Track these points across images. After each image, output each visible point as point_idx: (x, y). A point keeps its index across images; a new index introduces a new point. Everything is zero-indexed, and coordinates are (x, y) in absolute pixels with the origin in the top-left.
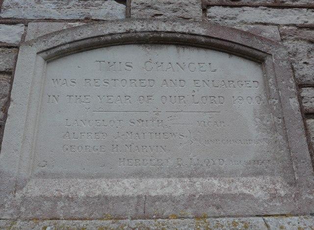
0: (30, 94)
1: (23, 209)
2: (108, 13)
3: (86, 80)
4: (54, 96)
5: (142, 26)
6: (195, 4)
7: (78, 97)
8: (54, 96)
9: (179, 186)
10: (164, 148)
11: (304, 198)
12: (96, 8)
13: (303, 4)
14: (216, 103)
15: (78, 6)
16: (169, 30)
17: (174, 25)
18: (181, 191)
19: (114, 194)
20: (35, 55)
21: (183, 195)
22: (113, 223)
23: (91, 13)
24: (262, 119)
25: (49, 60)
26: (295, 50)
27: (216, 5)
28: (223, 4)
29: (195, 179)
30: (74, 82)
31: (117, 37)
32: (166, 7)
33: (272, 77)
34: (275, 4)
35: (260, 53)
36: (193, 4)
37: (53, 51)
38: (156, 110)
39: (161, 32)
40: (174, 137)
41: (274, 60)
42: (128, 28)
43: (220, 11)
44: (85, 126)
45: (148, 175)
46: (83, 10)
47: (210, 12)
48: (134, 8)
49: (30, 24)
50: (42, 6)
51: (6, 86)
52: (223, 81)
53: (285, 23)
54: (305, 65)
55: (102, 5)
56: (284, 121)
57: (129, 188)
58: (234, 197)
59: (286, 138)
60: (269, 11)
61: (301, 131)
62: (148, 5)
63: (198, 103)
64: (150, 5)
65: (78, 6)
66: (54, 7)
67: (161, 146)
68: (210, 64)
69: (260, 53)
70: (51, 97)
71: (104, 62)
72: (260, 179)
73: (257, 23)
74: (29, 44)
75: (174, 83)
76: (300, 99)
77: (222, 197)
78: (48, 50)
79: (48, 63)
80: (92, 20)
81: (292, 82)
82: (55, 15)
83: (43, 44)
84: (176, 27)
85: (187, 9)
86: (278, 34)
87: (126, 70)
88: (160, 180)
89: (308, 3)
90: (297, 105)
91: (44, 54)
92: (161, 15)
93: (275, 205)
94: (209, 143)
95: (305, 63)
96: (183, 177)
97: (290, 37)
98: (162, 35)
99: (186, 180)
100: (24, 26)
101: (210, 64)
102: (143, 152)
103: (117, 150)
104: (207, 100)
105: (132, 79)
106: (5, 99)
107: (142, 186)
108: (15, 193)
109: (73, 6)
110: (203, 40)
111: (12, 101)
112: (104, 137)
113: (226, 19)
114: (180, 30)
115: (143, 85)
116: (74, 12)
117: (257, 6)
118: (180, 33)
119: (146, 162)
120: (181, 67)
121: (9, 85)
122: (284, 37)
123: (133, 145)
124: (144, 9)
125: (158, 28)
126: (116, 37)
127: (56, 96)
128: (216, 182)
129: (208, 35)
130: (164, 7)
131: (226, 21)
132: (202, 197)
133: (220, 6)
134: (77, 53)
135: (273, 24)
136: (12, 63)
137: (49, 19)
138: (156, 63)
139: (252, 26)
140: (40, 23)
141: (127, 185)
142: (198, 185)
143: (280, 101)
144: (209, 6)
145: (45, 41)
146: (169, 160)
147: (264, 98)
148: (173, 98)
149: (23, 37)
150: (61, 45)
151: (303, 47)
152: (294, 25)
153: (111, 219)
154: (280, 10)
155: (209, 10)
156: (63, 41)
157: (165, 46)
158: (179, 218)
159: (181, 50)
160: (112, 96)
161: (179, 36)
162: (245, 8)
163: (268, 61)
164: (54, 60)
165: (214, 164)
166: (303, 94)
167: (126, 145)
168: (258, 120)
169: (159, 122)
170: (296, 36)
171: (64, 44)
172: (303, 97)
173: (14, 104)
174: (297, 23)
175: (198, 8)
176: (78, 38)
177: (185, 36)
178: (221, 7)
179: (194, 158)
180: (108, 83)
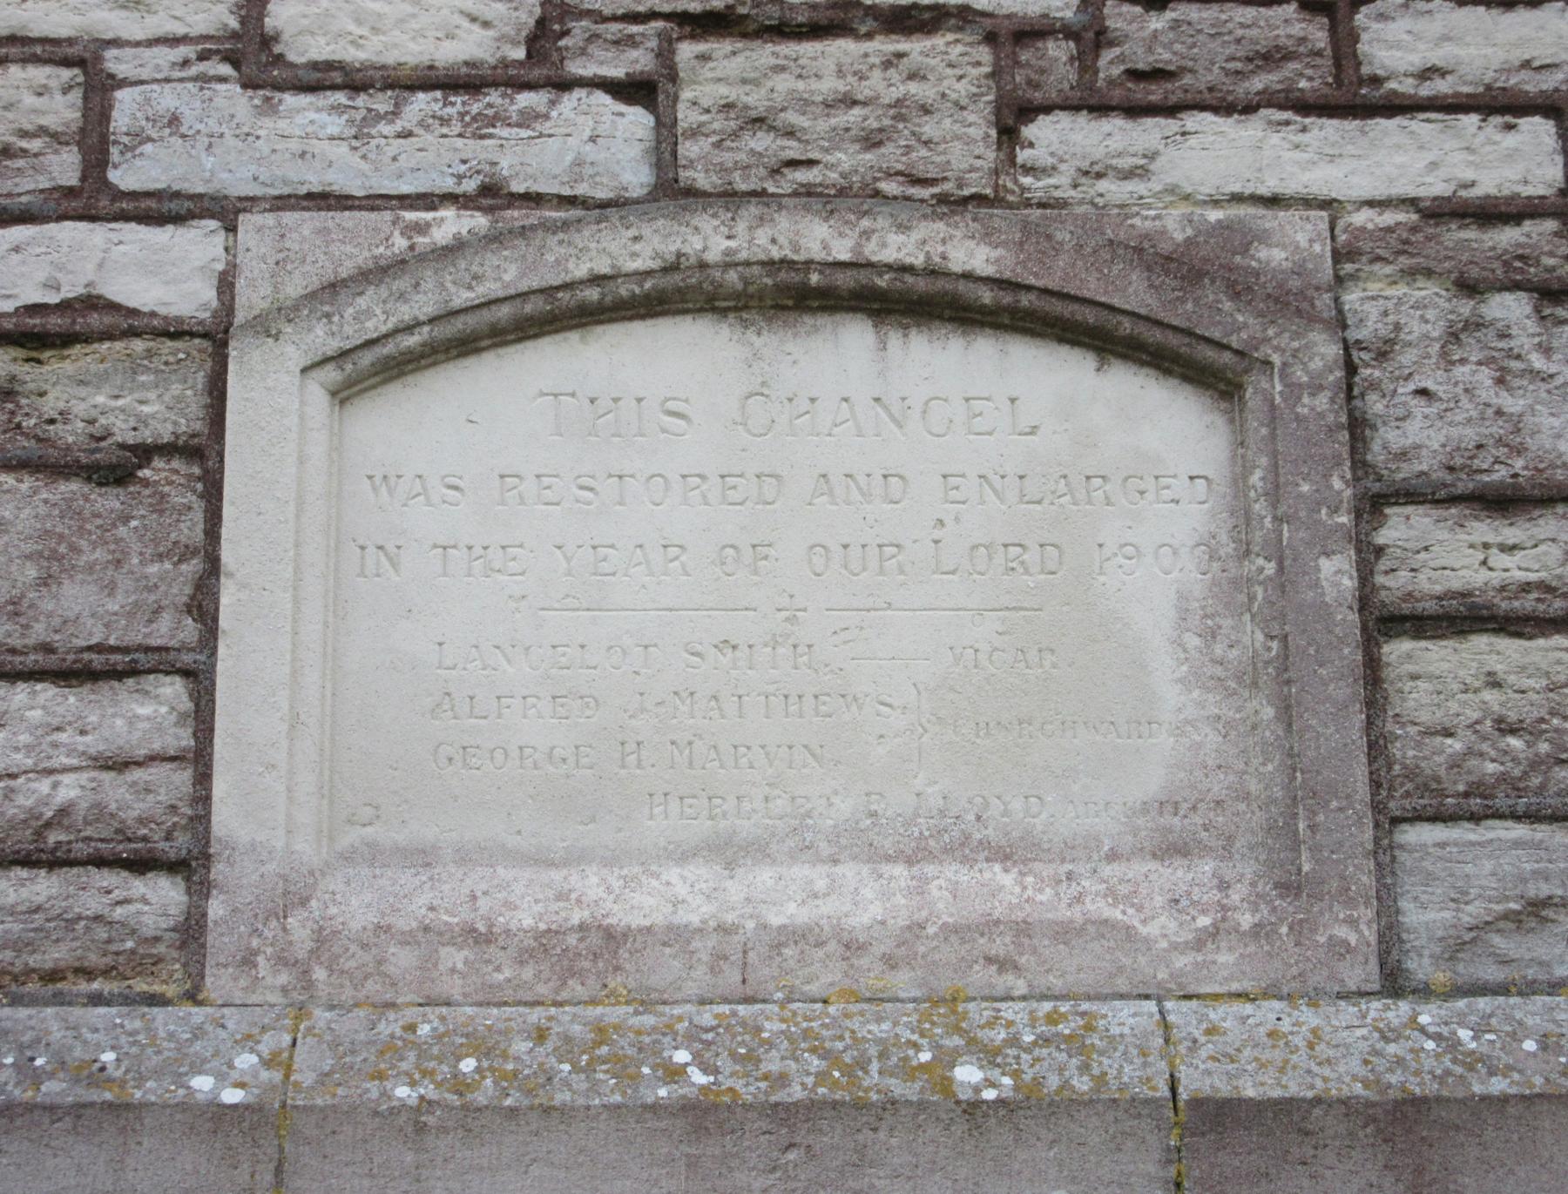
0: (297, 545)
1: (320, 974)
2: (579, 163)
3: (502, 477)
4: (380, 548)
5: (729, 237)
6: (964, 102)
7: (478, 551)
8: (380, 548)
9: (868, 893)
10: (818, 751)
11: (1322, 940)
12: (525, 133)
13: (1466, 89)
14: (1027, 572)
15: (444, 121)
16: (845, 256)
17: (867, 234)
18: (876, 911)
19: (637, 921)
20: (297, 380)
21: (883, 923)
22: (637, 1013)
23: (506, 164)
24: (1212, 635)
25: (343, 395)
26: (1384, 332)
27: (1063, 108)
28: (1092, 102)
29: (930, 869)
30: (456, 488)
31: (624, 290)
32: (833, 121)
33: (1264, 461)
34: (1339, 96)
35: (1227, 357)
36: (956, 103)
37: (367, 359)
38: (784, 601)
39: (809, 263)
40: (854, 708)
41: (1278, 388)
42: (671, 248)
43: (1077, 137)
44: (511, 670)
45: (760, 850)
46: (469, 147)
47: (1031, 145)
48: (695, 133)
49: (247, 222)
50: (282, 125)
51: (190, 508)
52: (1065, 477)
53: (1367, 194)
54: (1422, 401)
55: (547, 117)
56: (1286, 647)
57: (690, 899)
58: (1064, 933)
59: (1286, 713)
60: (1304, 130)
61: (1345, 690)
62: (754, 114)
63: (953, 572)
64: (760, 111)
65: (444, 121)
66: (333, 130)
67: (805, 747)
68: (1013, 400)
69: (1227, 357)
70: (371, 550)
71: (573, 395)
72: (1175, 875)
73: (1237, 198)
74: (264, 326)
75: (859, 489)
76: (1368, 556)
77: (1023, 930)
78: (344, 354)
79: (342, 402)
80: (512, 195)
81: (1337, 484)
82: (348, 171)
83: (320, 330)
84: (874, 239)
85: (929, 129)
86: (1323, 249)
87: (664, 431)
88: (801, 871)
89: (1489, 88)
90: (1349, 583)
91: (331, 374)
92: (811, 163)
93: (1214, 962)
94: (988, 734)
95: (1423, 392)
96: (888, 859)
97: (1377, 267)
98: (814, 278)
99: (899, 870)
100: (223, 233)
101: (1013, 400)
102: (736, 767)
103: (639, 760)
104: (990, 558)
105: (693, 472)
106: (193, 567)
107: (735, 890)
108: (285, 917)
109: (421, 123)
110: (987, 296)
111: (230, 575)
112: (588, 713)
113: (1099, 176)
114: (889, 255)
115: (733, 495)
116: (430, 156)
117: (1249, 109)
118: (889, 267)
119: (746, 806)
120: (891, 416)
121: (199, 506)
122: (1349, 267)
123: (698, 743)
124: (735, 135)
125: (796, 250)
126: (623, 292)
127: (390, 548)
128: (1008, 880)
129: (1007, 275)
130: (822, 125)
131: (1103, 185)
132: (949, 931)
133: (1075, 108)
134: (458, 356)
135: (1308, 202)
136: (195, 404)
137: (324, 196)
138: (790, 400)
139: (1214, 215)
140: (289, 217)
141: (682, 890)
142: (937, 892)
143: (1281, 569)
144: (1029, 112)
145: (328, 316)
146: (836, 800)
147: (1229, 549)
148: (855, 552)
149: (226, 284)
150: (396, 331)
151: (1431, 314)
152: (1412, 203)
153: (628, 1003)
154: (1352, 125)
155: (1029, 131)
156: (405, 313)
157: (823, 320)
158: (869, 1000)
159: (894, 338)
160: (612, 546)
161: (882, 282)
162: (1193, 120)
163: (1256, 388)
164: (374, 387)
165: (1005, 813)
166: (1383, 537)
167: (673, 743)
168: (1193, 641)
169: (799, 650)
170: (1404, 261)
171: (409, 329)
172: (1380, 551)
173: (243, 586)
174: (1422, 192)
175: (979, 126)
176: (463, 297)
177: (909, 279)
178: (1082, 118)
179: (930, 790)
180: (591, 489)
